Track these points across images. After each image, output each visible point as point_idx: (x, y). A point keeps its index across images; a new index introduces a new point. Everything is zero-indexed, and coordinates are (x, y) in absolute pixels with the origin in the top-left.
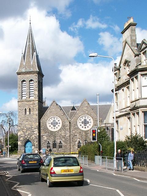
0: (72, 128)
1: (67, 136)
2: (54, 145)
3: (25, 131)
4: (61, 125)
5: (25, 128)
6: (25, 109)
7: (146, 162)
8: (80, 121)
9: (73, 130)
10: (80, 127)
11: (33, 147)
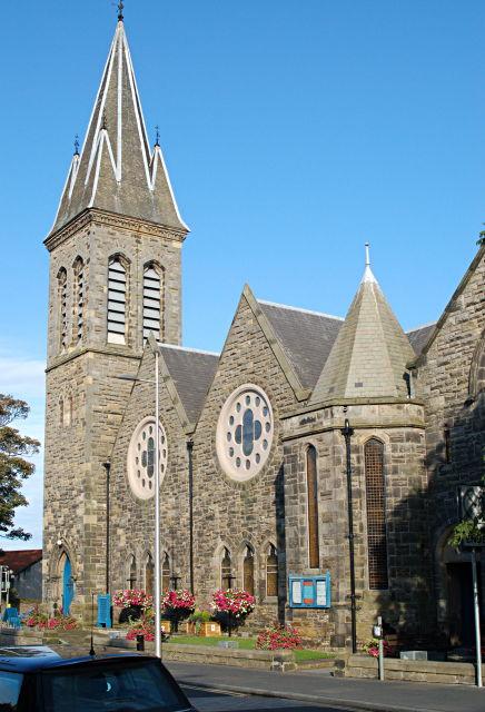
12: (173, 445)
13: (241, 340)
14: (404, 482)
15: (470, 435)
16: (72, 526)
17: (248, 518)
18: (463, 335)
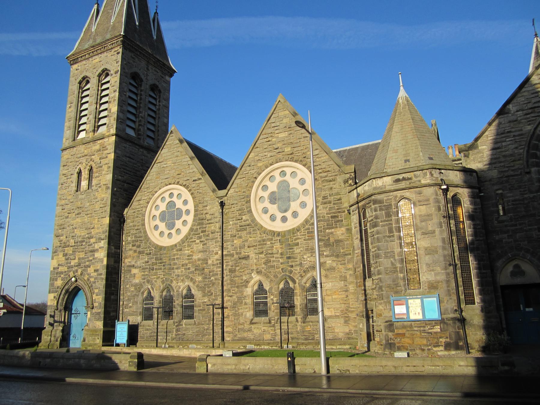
0: (231, 225)
1: (210, 262)
3: (69, 250)
4: (190, 219)
5: (72, 242)
7: (537, 165)
8: (261, 193)
9: (234, 232)
10: (264, 221)
11: (353, 329)
12: (200, 206)
14: (479, 227)
15: (525, 196)
17: (289, 258)
18: (513, 130)
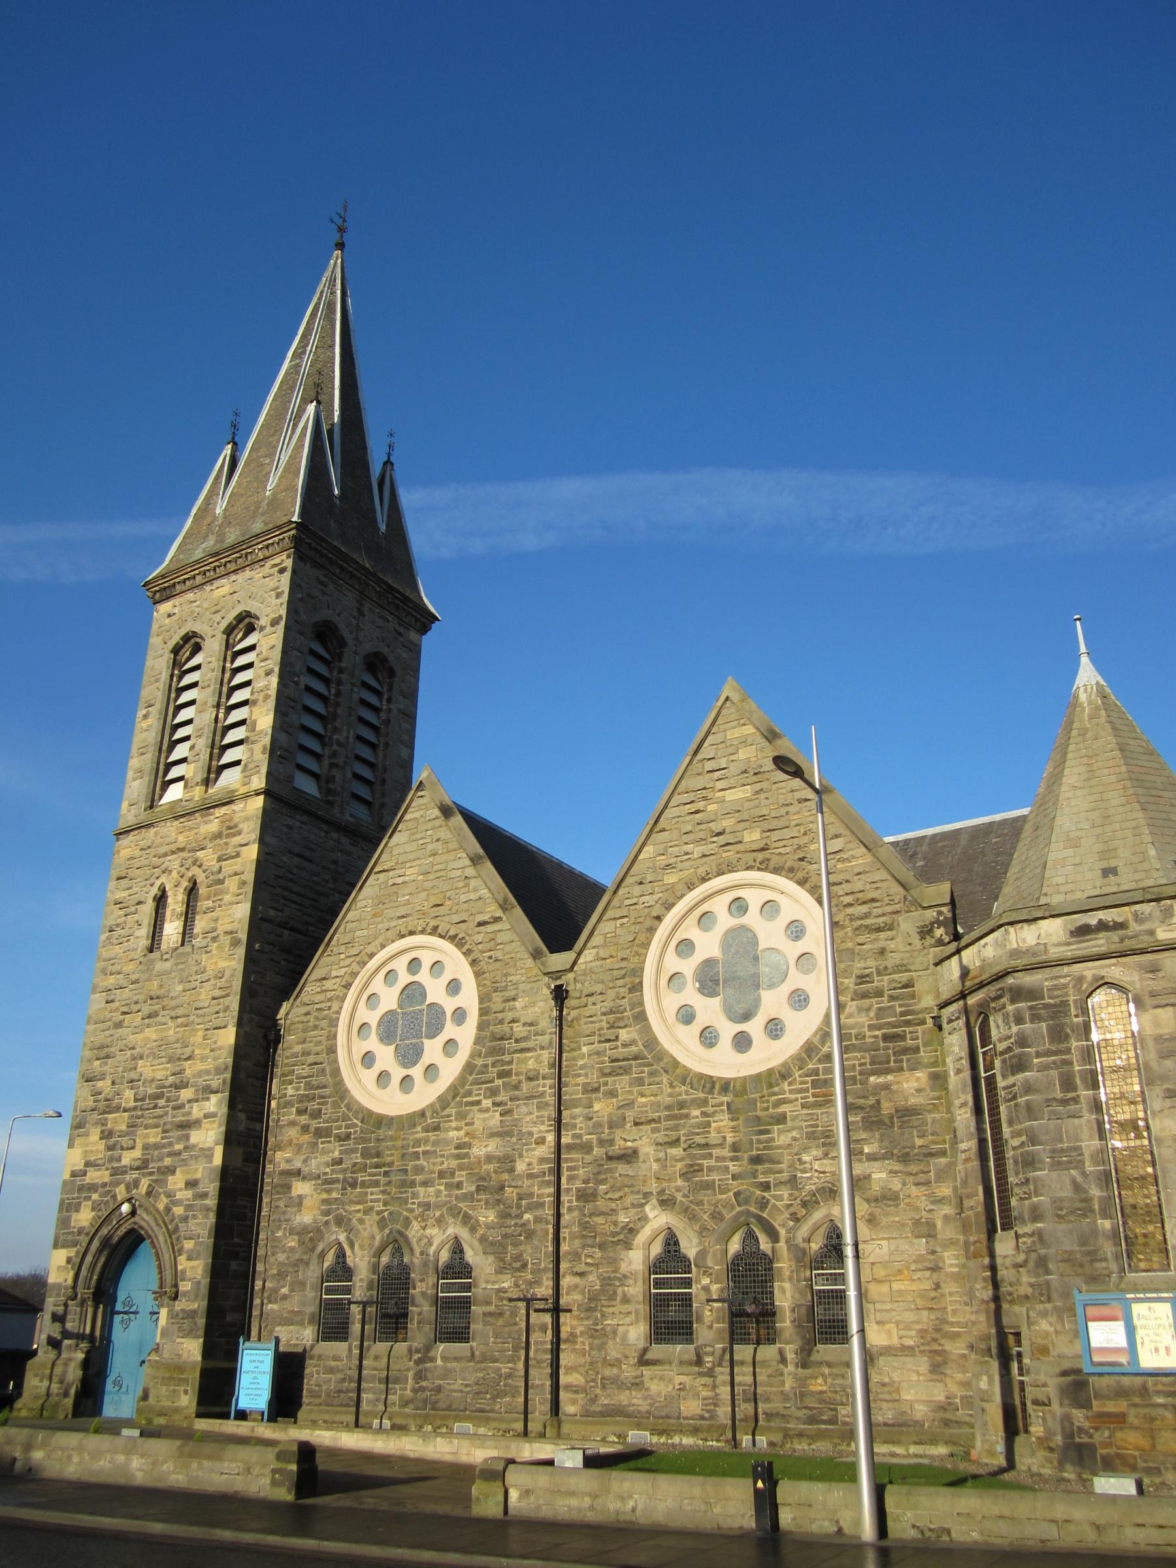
0: (585, 1057)
1: (521, 1167)
2: (393, 1287)
3: (118, 1122)
6: (161, 900)
8: (673, 963)
10: (682, 1045)
13: (720, 785)
16: (171, 1171)
17: (756, 1160)
